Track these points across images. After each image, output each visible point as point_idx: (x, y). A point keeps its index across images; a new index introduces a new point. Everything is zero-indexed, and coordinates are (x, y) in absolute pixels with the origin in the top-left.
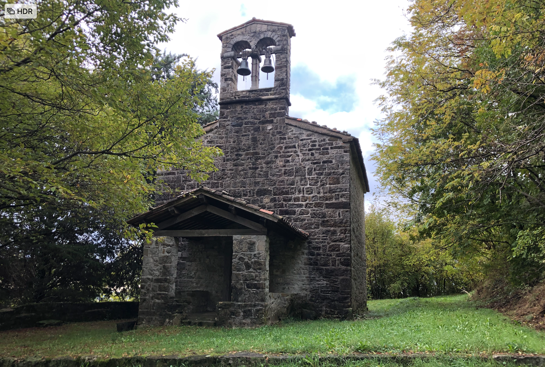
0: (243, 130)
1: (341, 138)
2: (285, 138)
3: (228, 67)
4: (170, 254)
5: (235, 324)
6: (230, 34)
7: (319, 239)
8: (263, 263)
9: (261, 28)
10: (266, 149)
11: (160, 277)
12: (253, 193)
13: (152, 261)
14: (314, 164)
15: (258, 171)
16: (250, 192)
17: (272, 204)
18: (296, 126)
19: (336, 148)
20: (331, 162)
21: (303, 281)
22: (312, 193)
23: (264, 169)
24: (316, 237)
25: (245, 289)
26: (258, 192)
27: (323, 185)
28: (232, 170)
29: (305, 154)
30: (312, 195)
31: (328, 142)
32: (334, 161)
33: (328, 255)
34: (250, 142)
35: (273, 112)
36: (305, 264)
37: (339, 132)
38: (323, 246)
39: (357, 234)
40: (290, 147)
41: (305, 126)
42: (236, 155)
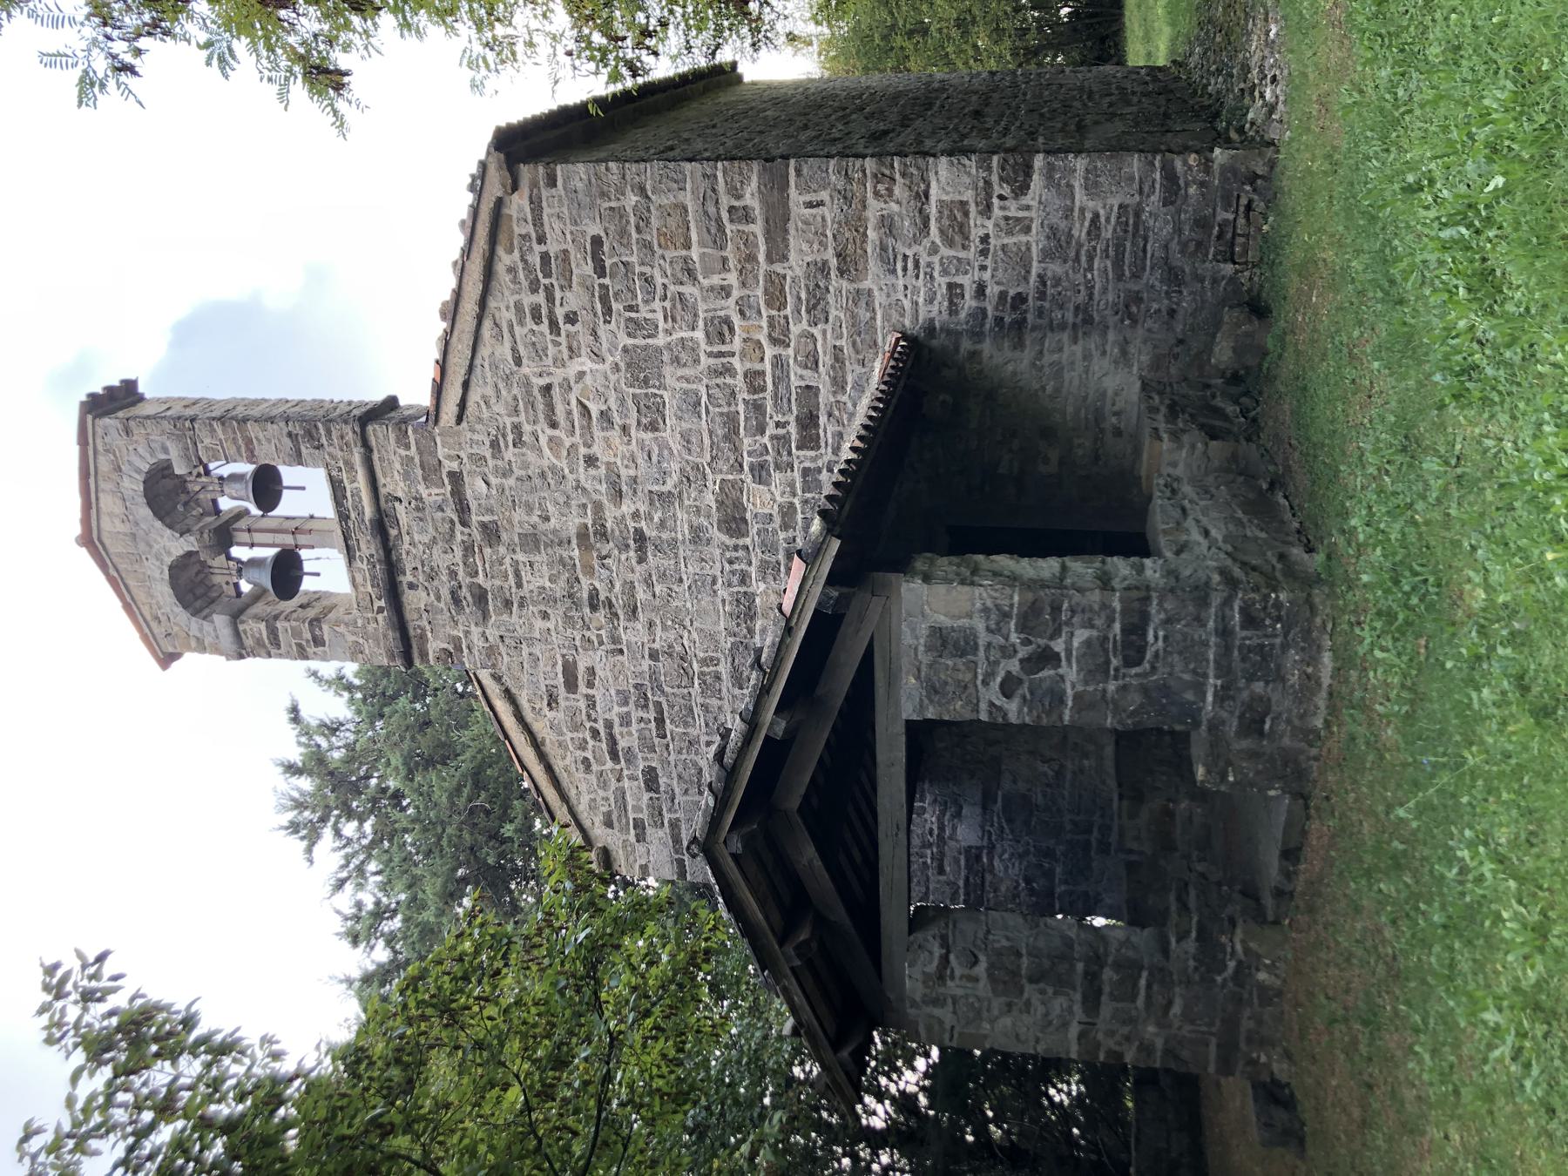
0: (498, 582)
1: (499, 203)
2: (517, 428)
3: (273, 632)
4: (982, 958)
5: (1302, 717)
6: (154, 625)
7: (916, 290)
8: (1030, 596)
9: (111, 515)
10: (562, 500)
11: (1078, 997)
12: (736, 548)
13: (1007, 1021)
14: (608, 311)
15: (650, 532)
16: (731, 562)
17: (777, 477)
18: (466, 385)
19: (538, 221)
20: (597, 241)
21: (1087, 357)
22: (727, 321)
23: (643, 508)
24: (907, 304)
25: (1145, 675)
26: (730, 532)
27: (690, 273)
28: (651, 624)
29: (570, 348)
30: (736, 320)
31: (516, 254)
32: (595, 229)
33: (984, 253)
34: (540, 558)
35: (419, 472)
36: (1019, 345)
37: (475, 211)
38: (945, 272)
39: (893, 116)
40: (550, 408)
41: (461, 349)
42: (594, 608)
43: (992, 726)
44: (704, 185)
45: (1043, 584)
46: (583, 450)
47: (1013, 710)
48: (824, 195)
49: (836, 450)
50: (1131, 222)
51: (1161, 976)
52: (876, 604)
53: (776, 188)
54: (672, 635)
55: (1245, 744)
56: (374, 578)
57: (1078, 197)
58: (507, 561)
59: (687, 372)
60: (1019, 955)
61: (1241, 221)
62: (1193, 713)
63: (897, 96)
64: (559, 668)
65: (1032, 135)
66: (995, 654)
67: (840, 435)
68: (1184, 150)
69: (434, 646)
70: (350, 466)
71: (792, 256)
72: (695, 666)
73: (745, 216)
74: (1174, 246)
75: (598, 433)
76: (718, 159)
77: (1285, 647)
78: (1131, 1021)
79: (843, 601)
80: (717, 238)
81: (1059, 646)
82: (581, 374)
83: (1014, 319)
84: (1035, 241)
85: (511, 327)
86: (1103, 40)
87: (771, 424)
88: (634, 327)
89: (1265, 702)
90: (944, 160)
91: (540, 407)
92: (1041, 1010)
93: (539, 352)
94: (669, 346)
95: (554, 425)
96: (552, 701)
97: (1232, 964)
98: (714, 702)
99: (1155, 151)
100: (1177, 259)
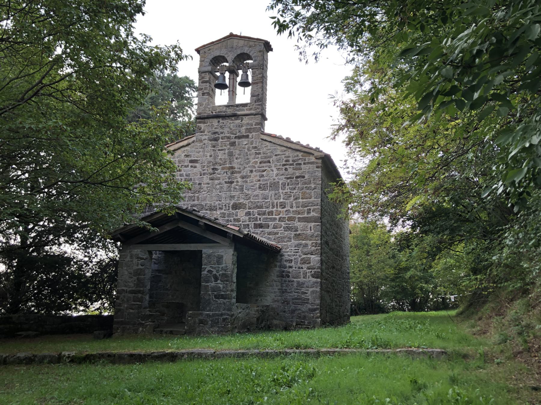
0: (220, 144)
2: (260, 153)
4: (143, 267)
6: (208, 49)
10: (242, 163)
11: (134, 289)
12: (229, 207)
13: (126, 273)
14: (288, 178)
17: (247, 218)
18: (270, 142)
19: (309, 163)
20: (304, 177)
23: (239, 184)
24: (288, 250)
25: (213, 299)
26: (233, 206)
28: (208, 184)
30: (285, 209)
31: (301, 157)
33: (299, 268)
34: (226, 156)
35: (249, 127)
36: (278, 276)
37: (311, 149)
38: (295, 259)
40: (265, 162)
42: (213, 169)
43: (201, 268)
44: (316, 203)
45: (232, 278)
46: (254, 170)
47: (204, 273)
48: (313, 231)
49: (253, 233)
50: (305, 301)
51: (140, 307)
52: (227, 244)
53: (314, 220)
54: (205, 189)
55: (197, 321)
56: (221, 112)
57: (311, 288)
58: (226, 148)
59: (273, 197)
60: (144, 275)
61: (305, 326)
62: (204, 310)
63: (341, 247)
64: (196, 159)
65: (326, 279)
66: (217, 269)
67: (257, 234)
68: (321, 314)
69: (202, 126)
70: (251, 109)
71: (299, 223)
72: (197, 195)
73: (309, 213)
74: (300, 311)
75: (258, 174)
76: (321, 206)
77: (219, 327)
78: (128, 301)
79: (229, 238)
80: (304, 206)
81: (219, 282)
82: (273, 171)
83: (284, 275)
84: (302, 280)
85: (284, 154)
86: (365, 309)
87: (260, 217)
88: (284, 185)
89: (207, 324)
90: (320, 258)
91: (265, 160)
92: (130, 281)
93: (278, 161)
94: (279, 193)
95: (260, 163)
96: (187, 156)
97: (143, 322)
98: (187, 199)
99: (321, 306)
100: (297, 312)
